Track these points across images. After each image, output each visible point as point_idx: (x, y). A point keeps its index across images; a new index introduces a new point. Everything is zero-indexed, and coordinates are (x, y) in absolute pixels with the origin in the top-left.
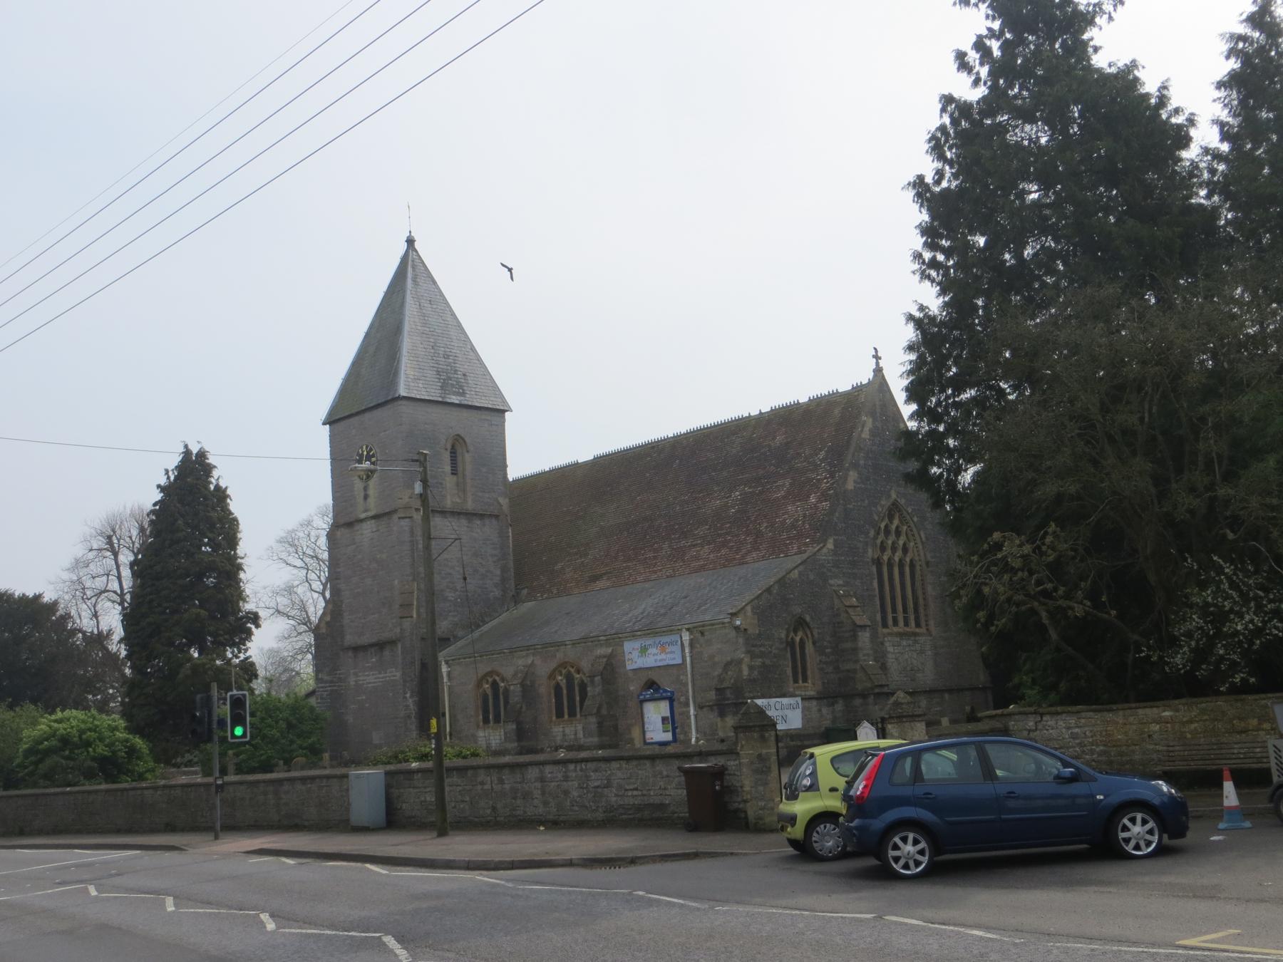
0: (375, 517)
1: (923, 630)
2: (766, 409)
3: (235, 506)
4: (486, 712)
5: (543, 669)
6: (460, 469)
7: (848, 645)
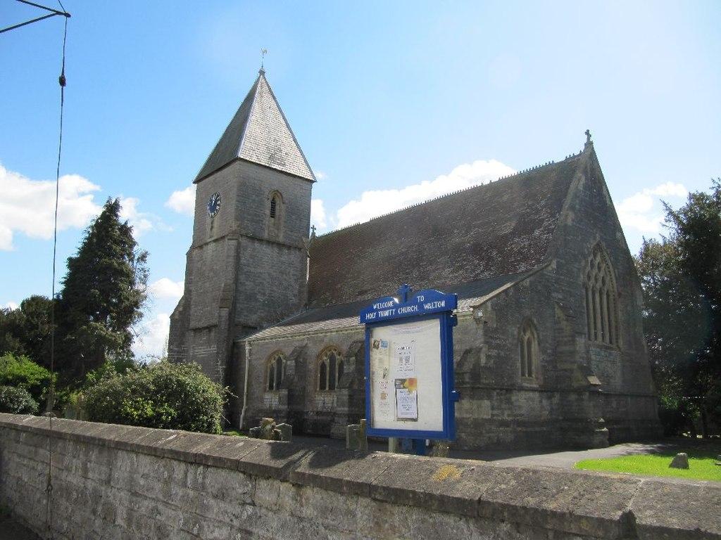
0: (215, 241)
1: (614, 346)
2: (495, 179)
3: (135, 234)
4: (272, 381)
5: (314, 350)
6: (277, 213)
7: (566, 348)
